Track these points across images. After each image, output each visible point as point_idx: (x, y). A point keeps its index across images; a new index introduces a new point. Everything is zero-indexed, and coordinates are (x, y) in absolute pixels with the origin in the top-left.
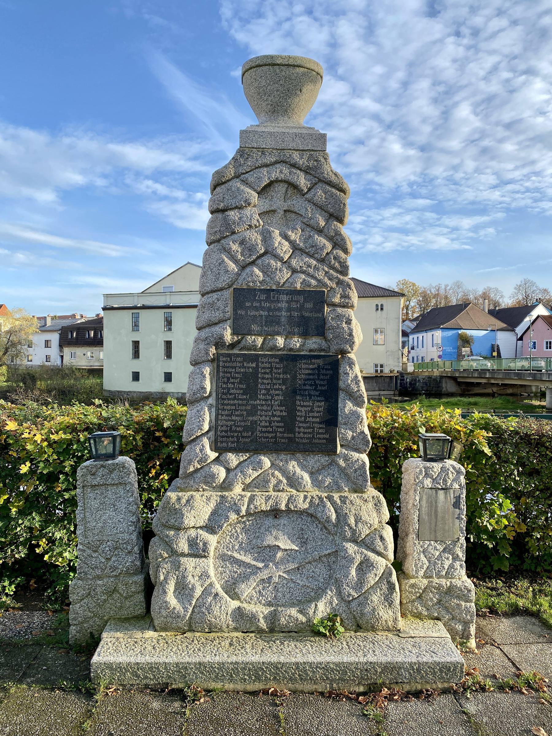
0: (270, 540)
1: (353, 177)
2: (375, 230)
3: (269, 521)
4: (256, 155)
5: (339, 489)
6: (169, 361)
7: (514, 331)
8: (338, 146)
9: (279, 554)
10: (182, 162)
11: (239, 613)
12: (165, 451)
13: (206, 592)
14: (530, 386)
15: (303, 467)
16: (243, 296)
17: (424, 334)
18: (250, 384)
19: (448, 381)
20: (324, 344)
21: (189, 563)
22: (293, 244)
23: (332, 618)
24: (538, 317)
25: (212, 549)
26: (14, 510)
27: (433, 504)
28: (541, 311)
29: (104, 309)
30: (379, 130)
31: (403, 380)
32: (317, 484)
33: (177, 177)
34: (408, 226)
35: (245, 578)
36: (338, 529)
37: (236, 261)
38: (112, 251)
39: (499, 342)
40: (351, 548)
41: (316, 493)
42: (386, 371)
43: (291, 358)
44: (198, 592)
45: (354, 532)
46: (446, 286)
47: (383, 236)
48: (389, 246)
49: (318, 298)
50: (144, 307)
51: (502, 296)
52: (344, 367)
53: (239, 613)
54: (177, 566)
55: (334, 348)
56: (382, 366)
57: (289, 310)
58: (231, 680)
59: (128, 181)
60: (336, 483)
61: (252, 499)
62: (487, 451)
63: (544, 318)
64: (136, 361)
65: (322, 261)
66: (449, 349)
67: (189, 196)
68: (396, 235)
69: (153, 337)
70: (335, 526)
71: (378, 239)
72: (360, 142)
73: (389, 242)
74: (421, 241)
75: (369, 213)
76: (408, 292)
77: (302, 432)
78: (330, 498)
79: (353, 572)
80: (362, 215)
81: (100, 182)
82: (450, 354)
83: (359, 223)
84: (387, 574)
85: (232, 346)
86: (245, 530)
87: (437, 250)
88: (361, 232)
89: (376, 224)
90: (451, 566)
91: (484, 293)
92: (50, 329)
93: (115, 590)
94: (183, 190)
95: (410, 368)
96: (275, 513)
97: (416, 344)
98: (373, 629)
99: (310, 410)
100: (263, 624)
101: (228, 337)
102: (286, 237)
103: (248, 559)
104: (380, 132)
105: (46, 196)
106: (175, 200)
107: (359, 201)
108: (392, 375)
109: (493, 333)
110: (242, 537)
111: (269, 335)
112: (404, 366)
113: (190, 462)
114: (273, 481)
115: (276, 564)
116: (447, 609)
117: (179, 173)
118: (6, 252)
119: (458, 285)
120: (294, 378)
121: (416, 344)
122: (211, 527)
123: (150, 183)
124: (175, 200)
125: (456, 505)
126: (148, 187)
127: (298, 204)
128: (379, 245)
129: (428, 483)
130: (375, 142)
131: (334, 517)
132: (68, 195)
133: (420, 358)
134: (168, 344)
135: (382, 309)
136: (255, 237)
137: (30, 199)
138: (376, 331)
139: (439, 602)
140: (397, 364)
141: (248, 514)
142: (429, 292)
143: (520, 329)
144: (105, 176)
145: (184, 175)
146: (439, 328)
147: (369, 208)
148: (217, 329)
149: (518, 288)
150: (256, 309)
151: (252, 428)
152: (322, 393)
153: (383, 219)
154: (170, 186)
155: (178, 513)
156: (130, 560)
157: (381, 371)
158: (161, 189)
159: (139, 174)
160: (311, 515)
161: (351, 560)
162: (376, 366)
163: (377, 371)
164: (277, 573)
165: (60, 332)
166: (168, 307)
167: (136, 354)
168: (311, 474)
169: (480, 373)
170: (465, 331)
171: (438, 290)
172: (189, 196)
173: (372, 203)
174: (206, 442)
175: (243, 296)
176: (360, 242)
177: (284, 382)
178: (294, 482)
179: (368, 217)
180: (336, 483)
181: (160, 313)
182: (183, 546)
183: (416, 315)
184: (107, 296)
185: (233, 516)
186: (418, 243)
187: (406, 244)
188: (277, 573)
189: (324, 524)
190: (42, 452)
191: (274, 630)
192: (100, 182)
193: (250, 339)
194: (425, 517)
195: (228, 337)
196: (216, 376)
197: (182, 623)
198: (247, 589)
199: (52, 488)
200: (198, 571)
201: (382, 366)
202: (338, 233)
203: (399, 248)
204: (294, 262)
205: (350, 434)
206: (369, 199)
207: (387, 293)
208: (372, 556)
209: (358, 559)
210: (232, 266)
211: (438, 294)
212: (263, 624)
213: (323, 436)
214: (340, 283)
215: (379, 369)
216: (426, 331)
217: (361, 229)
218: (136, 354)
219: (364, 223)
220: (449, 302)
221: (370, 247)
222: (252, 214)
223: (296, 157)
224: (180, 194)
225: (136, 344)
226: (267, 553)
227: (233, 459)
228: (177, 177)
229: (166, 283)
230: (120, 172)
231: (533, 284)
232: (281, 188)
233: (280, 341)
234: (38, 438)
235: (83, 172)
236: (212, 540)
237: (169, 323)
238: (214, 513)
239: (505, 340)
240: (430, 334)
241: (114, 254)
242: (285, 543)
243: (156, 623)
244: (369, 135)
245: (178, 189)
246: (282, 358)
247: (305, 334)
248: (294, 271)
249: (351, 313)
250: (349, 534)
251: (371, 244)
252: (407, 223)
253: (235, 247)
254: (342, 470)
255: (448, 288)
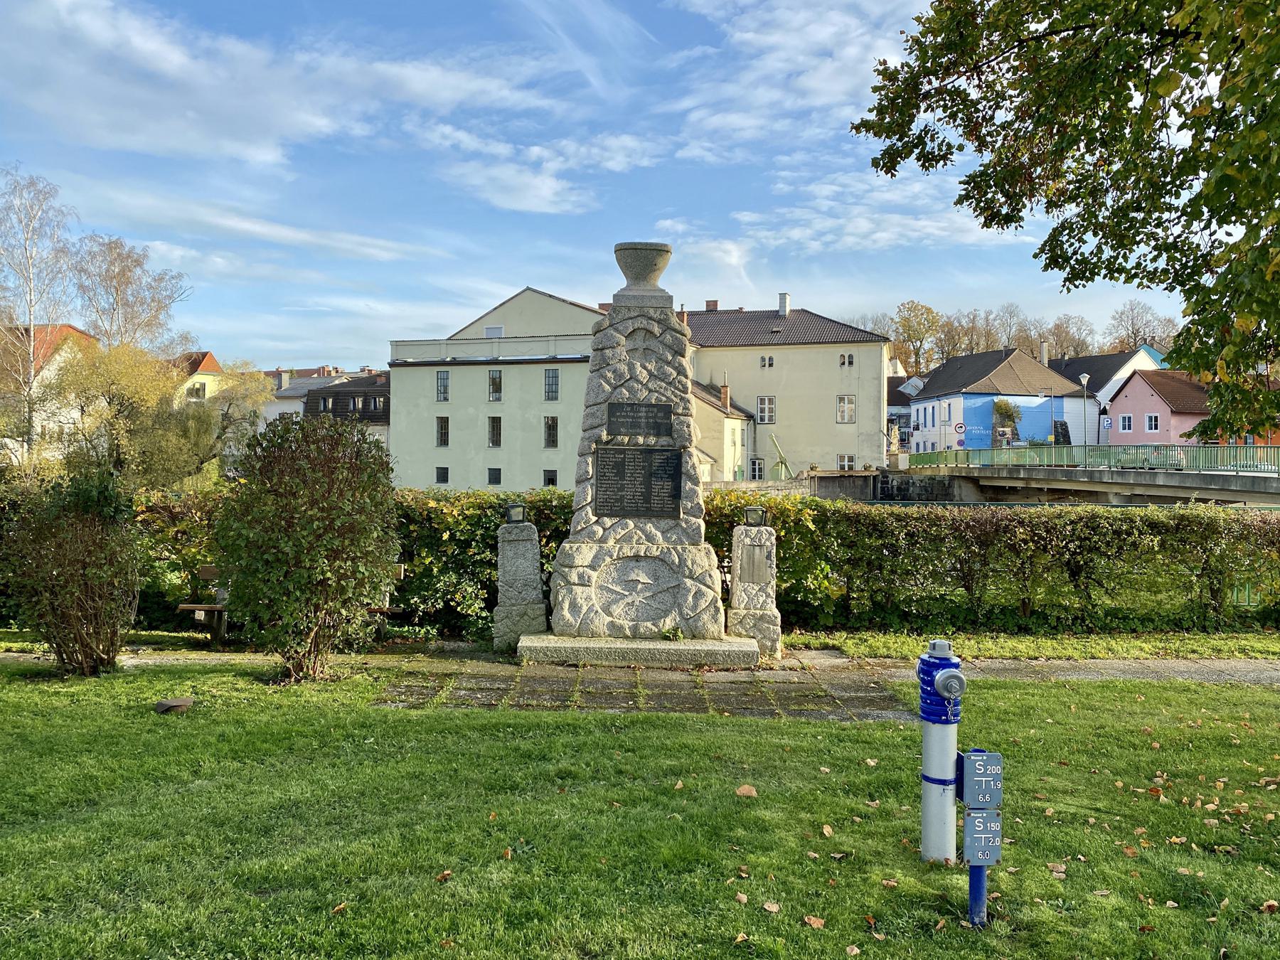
0: (633, 576)
1: (814, 115)
2: (856, 210)
3: (633, 564)
4: (624, 311)
5: (682, 543)
6: (496, 450)
7: (1094, 397)
8: (787, 60)
9: (640, 586)
10: (505, 93)
11: (612, 625)
12: (554, 524)
13: (590, 609)
14: (1106, 493)
15: (657, 528)
16: (614, 408)
17: (936, 403)
18: (620, 468)
19: (963, 484)
20: (671, 442)
21: (578, 590)
22: (650, 373)
23: (675, 629)
24: (1134, 373)
25: (594, 581)
26: (435, 570)
27: (751, 558)
28: (1143, 362)
29: (391, 365)
30: (860, 31)
31: (887, 483)
32: (666, 539)
33: (495, 118)
34: (919, 203)
35: (616, 601)
36: (679, 569)
37: (610, 384)
38: (382, 250)
39: (1066, 419)
40: (689, 582)
41: (665, 545)
42: (858, 466)
43: (648, 451)
44: (585, 609)
45: (691, 571)
46: (988, 313)
47: (872, 220)
48: (884, 237)
49: (667, 410)
50: (455, 363)
51: (1091, 332)
52: (685, 458)
53: (612, 625)
54: (571, 591)
55: (678, 444)
56: (851, 459)
57: (647, 418)
58: (607, 659)
59: (408, 127)
60: (680, 539)
61: (620, 549)
62: (812, 527)
63: (1144, 375)
64: (443, 450)
65: (670, 384)
66: (977, 430)
67: (518, 152)
68: (896, 218)
69: (471, 410)
70: (679, 566)
71: (863, 225)
72: (826, 53)
73: (884, 231)
74: (943, 229)
75: (842, 178)
76: (919, 324)
77: (655, 503)
78: (675, 549)
79: (690, 599)
80: (832, 183)
81: (360, 130)
82: (981, 438)
83: (827, 198)
84: (714, 601)
85: (607, 443)
86: (617, 570)
87: (972, 245)
88: (831, 214)
89: (858, 199)
90: (765, 602)
91: (1057, 327)
92: (287, 394)
93: (525, 614)
94: (507, 142)
95: (903, 463)
96: (637, 558)
97: (921, 420)
98: (704, 638)
99: (662, 488)
100: (628, 632)
101: (605, 437)
102: (645, 368)
103: (618, 589)
104: (862, 35)
105: (265, 156)
106: (492, 160)
107: (827, 158)
108: (867, 474)
109: (1056, 402)
110: (614, 574)
111: (632, 435)
112: (893, 458)
113: (578, 523)
114: (636, 537)
115: (638, 593)
116: (760, 630)
117: (499, 112)
118: (193, 253)
119: (1011, 311)
120: (650, 465)
121: (921, 420)
122: (593, 567)
123: (448, 129)
124: (492, 160)
125: (769, 557)
126: (444, 137)
127: (653, 344)
128: (865, 236)
129: (748, 541)
130: (852, 51)
131: (677, 561)
132: (307, 153)
133: (929, 445)
134: (495, 423)
135: (851, 363)
136: (623, 368)
137: (236, 163)
138: (841, 399)
139: (755, 625)
140: (876, 455)
141: (618, 558)
142: (956, 324)
143: (1104, 395)
144: (367, 118)
145: (507, 114)
146: (959, 392)
147: (845, 170)
148: (596, 431)
149: (1119, 317)
150: (624, 417)
151: (621, 499)
152: (670, 476)
153: (872, 190)
154: (484, 136)
155: (571, 557)
156: (536, 594)
157: (851, 468)
158: (467, 140)
159: (428, 115)
160: (661, 560)
161: (689, 591)
162: (842, 458)
163: (842, 467)
164: (638, 599)
165: (304, 400)
166: (495, 362)
167: (443, 440)
168: (663, 533)
169: (1010, 471)
170: (1005, 398)
171: (973, 321)
172: (518, 152)
173: (850, 161)
174: (589, 509)
175: (614, 408)
176: (830, 231)
177: (644, 468)
178: (650, 538)
179: (844, 186)
180: (680, 539)
181: (483, 374)
182: (574, 578)
183: (933, 366)
184: (396, 344)
185: (608, 559)
186: (937, 232)
187: (916, 234)
188: (638, 599)
189: (670, 566)
190: (457, 523)
191: (636, 636)
192: (360, 130)
193: (619, 438)
194: (745, 566)
195: (605, 437)
196: (596, 464)
197: (574, 631)
198: (618, 609)
199: (465, 552)
200: (584, 596)
201: (851, 459)
202: (681, 365)
203: (903, 242)
204: (650, 385)
205: (689, 505)
206: (846, 155)
207: (859, 336)
208: (703, 588)
209: (694, 590)
210: (607, 387)
211: (973, 327)
212: (628, 632)
213: (669, 506)
214: (682, 399)
215: (846, 463)
216: (938, 397)
217: (831, 208)
218: (443, 440)
219: (837, 197)
220: (996, 341)
221: (850, 240)
222: (622, 352)
223: (652, 312)
224: (503, 149)
225: (443, 423)
226: (631, 585)
227: (608, 522)
228: (495, 118)
229: (489, 323)
230: (395, 110)
231: (1147, 309)
232: (642, 333)
233: (641, 440)
234: (455, 513)
235: (330, 112)
236: (594, 575)
237: (496, 386)
238: (595, 557)
239: (1077, 414)
240: (945, 403)
241: (385, 256)
242: (643, 578)
243: (556, 631)
244: (842, 40)
245: (498, 141)
246: (641, 451)
247: (658, 435)
248: (650, 391)
249: (691, 420)
250: (687, 573)
251: (849, 234)
252: (916, 197)
253: (609, 375)
254: (684, 530)
255: (991, 317)
